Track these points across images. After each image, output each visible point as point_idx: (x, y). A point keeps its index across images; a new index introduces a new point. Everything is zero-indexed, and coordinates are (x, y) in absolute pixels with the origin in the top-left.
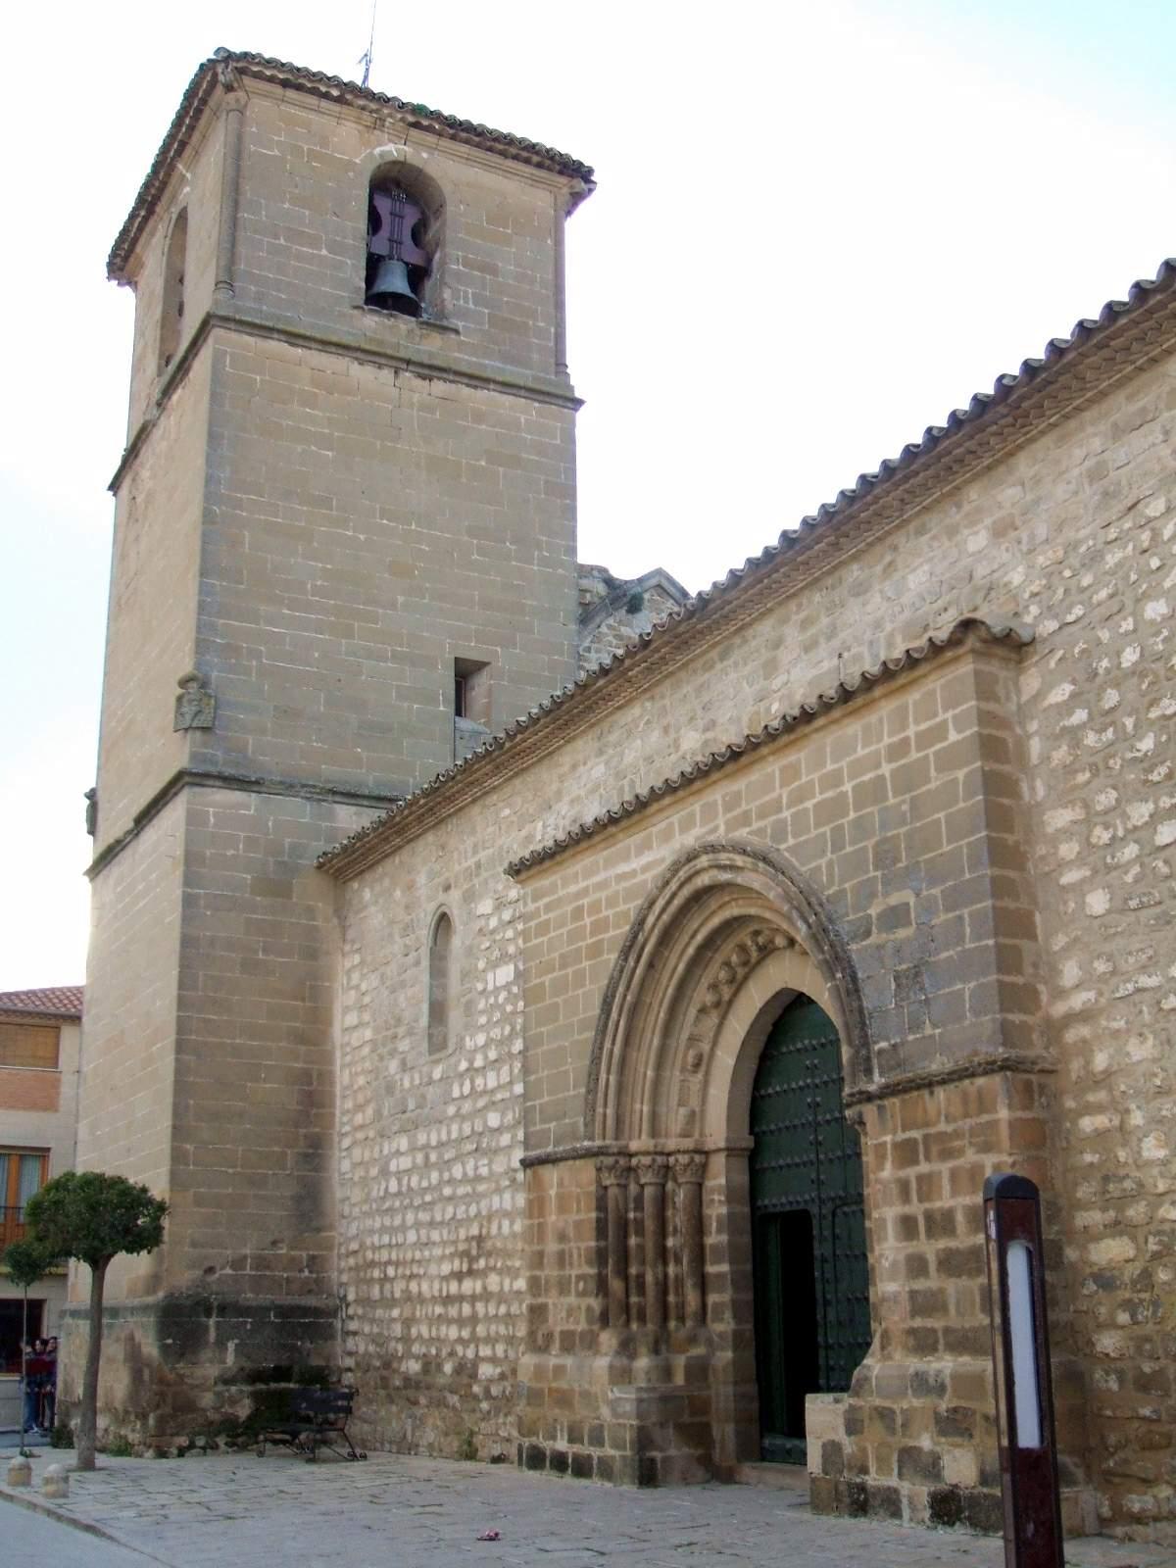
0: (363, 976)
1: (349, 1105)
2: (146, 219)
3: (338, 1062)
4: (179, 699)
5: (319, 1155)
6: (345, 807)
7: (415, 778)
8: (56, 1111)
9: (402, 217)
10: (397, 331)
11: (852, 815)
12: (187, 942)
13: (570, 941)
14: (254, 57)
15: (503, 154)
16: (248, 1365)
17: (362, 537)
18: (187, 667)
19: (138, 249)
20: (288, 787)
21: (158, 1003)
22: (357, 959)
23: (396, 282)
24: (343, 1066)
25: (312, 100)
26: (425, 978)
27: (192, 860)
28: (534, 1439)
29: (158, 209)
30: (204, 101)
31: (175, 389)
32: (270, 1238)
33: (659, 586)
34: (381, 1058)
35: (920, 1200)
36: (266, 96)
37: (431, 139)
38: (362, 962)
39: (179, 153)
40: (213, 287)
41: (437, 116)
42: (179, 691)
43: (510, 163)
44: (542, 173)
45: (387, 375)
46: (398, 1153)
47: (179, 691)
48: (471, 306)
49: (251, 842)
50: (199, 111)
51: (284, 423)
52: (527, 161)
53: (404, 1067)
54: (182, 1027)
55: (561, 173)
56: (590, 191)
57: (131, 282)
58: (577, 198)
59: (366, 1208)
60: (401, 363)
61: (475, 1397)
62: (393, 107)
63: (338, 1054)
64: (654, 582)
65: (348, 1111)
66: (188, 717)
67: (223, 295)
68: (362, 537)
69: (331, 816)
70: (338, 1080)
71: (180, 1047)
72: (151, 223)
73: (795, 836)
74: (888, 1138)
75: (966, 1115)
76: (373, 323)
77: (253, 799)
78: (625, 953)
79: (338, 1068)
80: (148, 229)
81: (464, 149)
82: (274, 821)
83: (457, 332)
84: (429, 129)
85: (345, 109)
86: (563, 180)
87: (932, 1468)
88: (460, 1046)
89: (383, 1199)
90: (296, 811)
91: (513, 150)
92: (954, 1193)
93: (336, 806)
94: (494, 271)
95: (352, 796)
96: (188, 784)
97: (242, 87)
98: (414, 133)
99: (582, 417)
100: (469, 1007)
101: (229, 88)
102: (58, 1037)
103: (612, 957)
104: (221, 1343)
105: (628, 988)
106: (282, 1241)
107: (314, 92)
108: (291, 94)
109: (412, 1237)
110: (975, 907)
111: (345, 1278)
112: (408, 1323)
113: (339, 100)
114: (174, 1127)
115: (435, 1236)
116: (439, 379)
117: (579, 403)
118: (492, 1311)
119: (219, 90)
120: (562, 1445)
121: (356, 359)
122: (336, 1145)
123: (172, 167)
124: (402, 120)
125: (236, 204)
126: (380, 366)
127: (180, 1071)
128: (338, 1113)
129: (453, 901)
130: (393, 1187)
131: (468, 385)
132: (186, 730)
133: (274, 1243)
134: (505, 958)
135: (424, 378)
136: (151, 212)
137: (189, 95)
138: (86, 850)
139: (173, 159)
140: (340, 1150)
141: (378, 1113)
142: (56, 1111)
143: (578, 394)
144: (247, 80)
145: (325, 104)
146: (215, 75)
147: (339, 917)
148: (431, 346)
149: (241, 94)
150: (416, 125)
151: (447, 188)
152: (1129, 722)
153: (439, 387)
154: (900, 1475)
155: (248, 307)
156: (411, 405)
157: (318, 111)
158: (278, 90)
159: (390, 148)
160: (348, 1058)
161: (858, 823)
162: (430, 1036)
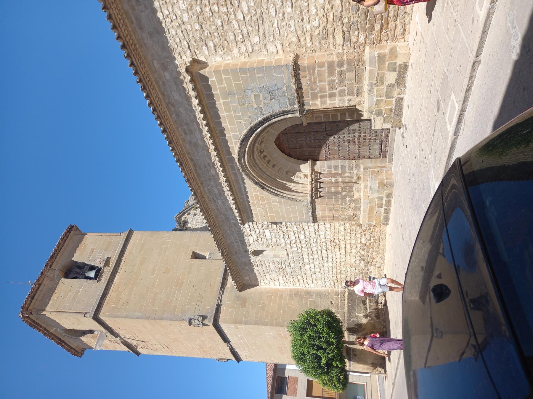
1: (298, 284)
2: (65, 343)
11: (232, 113)
13: (260, 207)
16: (363, 310)
19: (73, 347)
23: (92, 274)
25: (39, 292)
27: (235, 322)
28: (382, 219)
30: (34, 321)
35: (326, 92)
39: (48, 331)
43: (65, 244)
58: (77, 229)
61: (370, 244)
66: (199, 323)
67: (88, 315)
73: (237, 132)
74: (311, 102)
75: (306, 77)
78: (263, 188)
80: (68, 343)
86: (72, 232)
87: (391, 86)
92: (324, 81)
103: (265, 193)
104: (357, 317)
105: (272, 188)
107: (37, 291)
108: (35, 297)
109: (330, 264)
111: (341, 287)
112: (351, 266)
113: (40, 285)
115: (330, 256)
118: (349, 238)
119: (31, 316)
120: (382, 210)
123: (52, 334)
128: (300, 288)
134: (264, 232)
136: (64, 342)
145: (40, 289)
146: (27, 317)
150: (51, 266)
152: (213, 27)
154: (393, 98)
155: (92, 310)
157: (41, 291)
161: (235, 112)
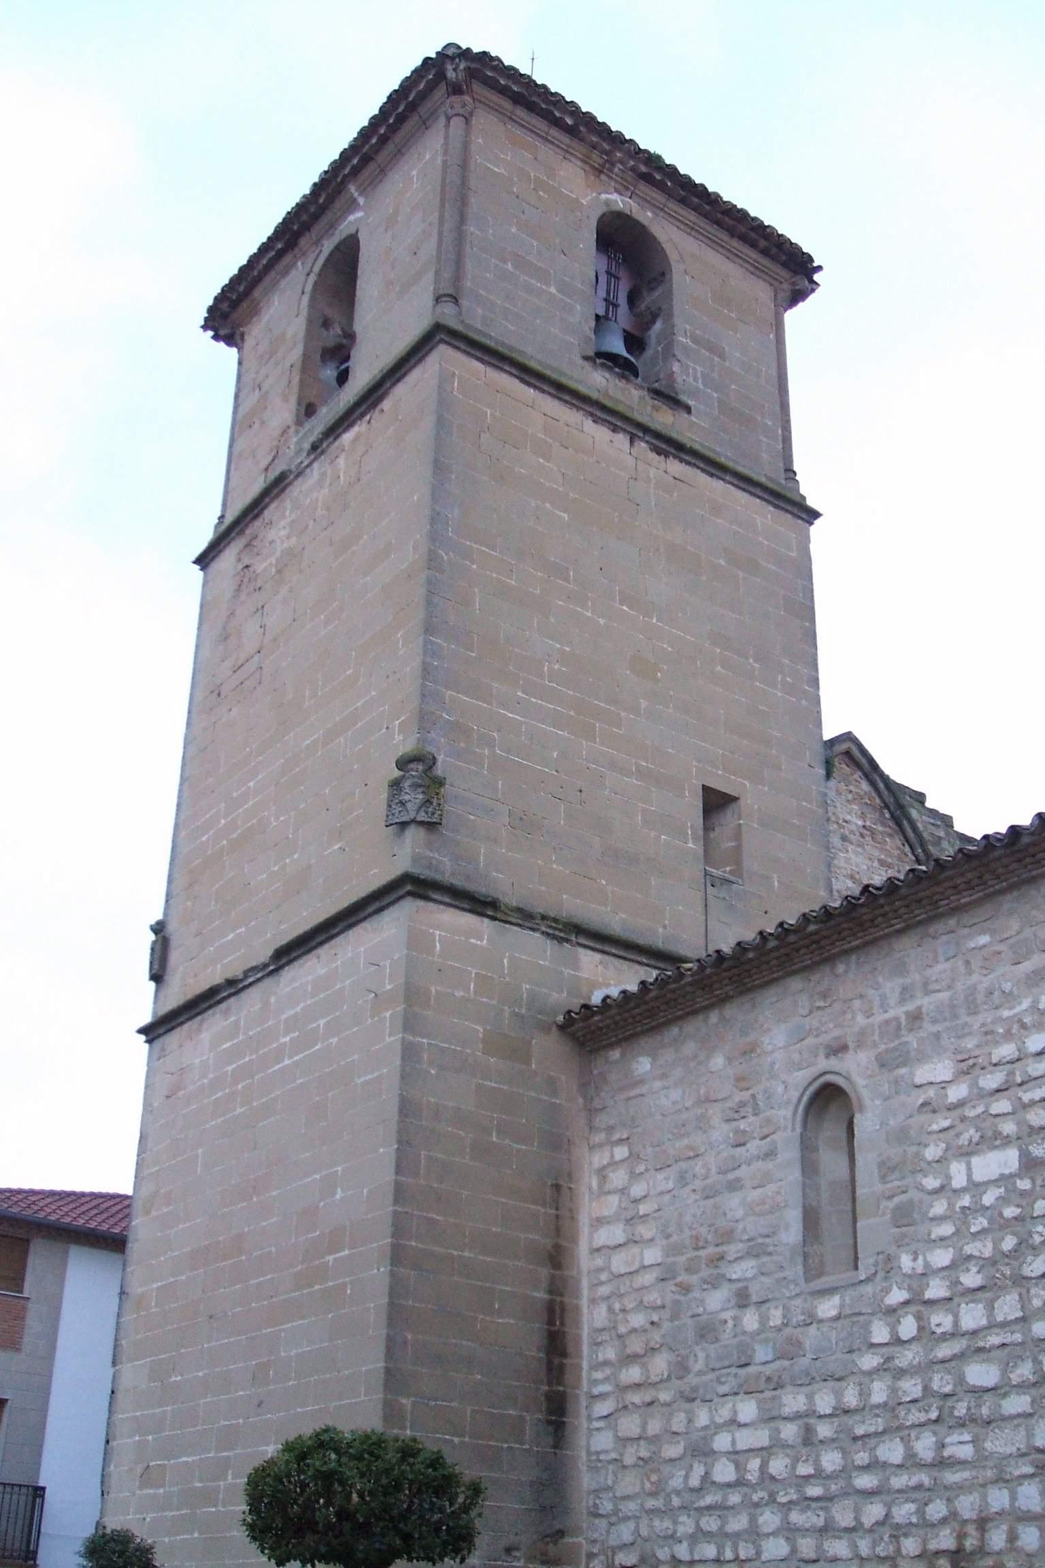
0: (634, 1176)
2: (281, 254)
3: (585, 1292)
4: (396, 785)
5: (564, 1423)
6: (590, 952)
7: (665, 927)
8: (18, 1350)
9: (617, 278)
10: (630, 396)
12: (406, 1108)
14: (492, 59)
15: (732, 233)
17: (602, 621)
18: (404, 744)
19: (257, 293)
20: (526, 918)
21: (339, 1194)
22: (621, 1152)
24: (593, 1301)
26: (795, 1174)
29: (303, 242)
31: (351, 425)
32: (503, 1543)
33: (848, 753)
34: (686, 1289)
36: (497, 110)
37: (659, 197)
38: (634, 1157)
39: (356, 171)
40: (431, 303)
41: (672, 171)
42: (397, 773)
44: (765, 262)
45: (622, 440)
46: (734, 1423)
47: (397, 773)
48: (701, 386)
49: (481, 979)
50: (402, 119)
51: (517, 469)
52: (753, 245)
53: (742, 1299)
54: (399, 1228)
55: (784, 265)
56: (813, 290)
57: (230, 340)
58: (797, 297)
59: (651, 1503)
60: (638, 430)
62: (628, 152)
63: (585, 1283)
64: (844, 747)
65: (606, 1363)
68: (602, 621)
69: (576, 966)
70: (585, 1319)
71: (397, 1255)
72: (287, 259)
76: (598, 381)
77: (485, 926)
79: (584, 1302)
81: (692, 216)
82: (511, 958)
83: (688, 410)
84: (660, 186)
85: (575, 144)
88: (888, 1265)
89: (698, 1490)
90: (533, 949)
91: (742, 229)
93: (581, 950)
94: (722, 356)
95: (602, 940)
96: (409, 894)
97: (470, 92)
98: (643, 187)
99: (817, 530)
100: (904, 1216)
101: (456, 90)
102: (25, 1253)
106: (517, 1549)
108: (521, 113)
110: (338, 1255)
114: (388, 1371)
116: (675, 457)
117: (814, 515)
121: (592, 414)
122: (583, 1412)
123: (341, 188)
124: (633, 169)
125: (462, 219)
126: (615, 429)
127: (396, 1290)
129: (855, 1070)
130: (724, 1472)
131: (703, 470)
132: (403, 825)
133: (508, 1550)
134: (992, 1140)
135: (659, 452)
137: (395, 98)
138: (142, 1004)
139: (345, 176)
140: (590, 1418)
141: (681, 1368)
142: (18, 1350)
143: (811, 502)
144: (477, 87)
145: (555, 132)
147: (585, 1097)
148: (664, 419)
149: (467, 98)
151: (673, 256)
153: (675, 467)
156: (648, 480)
158: (507, 104)
159: (615, 197)
160: (604, 1290)
162: (806, 1256)
